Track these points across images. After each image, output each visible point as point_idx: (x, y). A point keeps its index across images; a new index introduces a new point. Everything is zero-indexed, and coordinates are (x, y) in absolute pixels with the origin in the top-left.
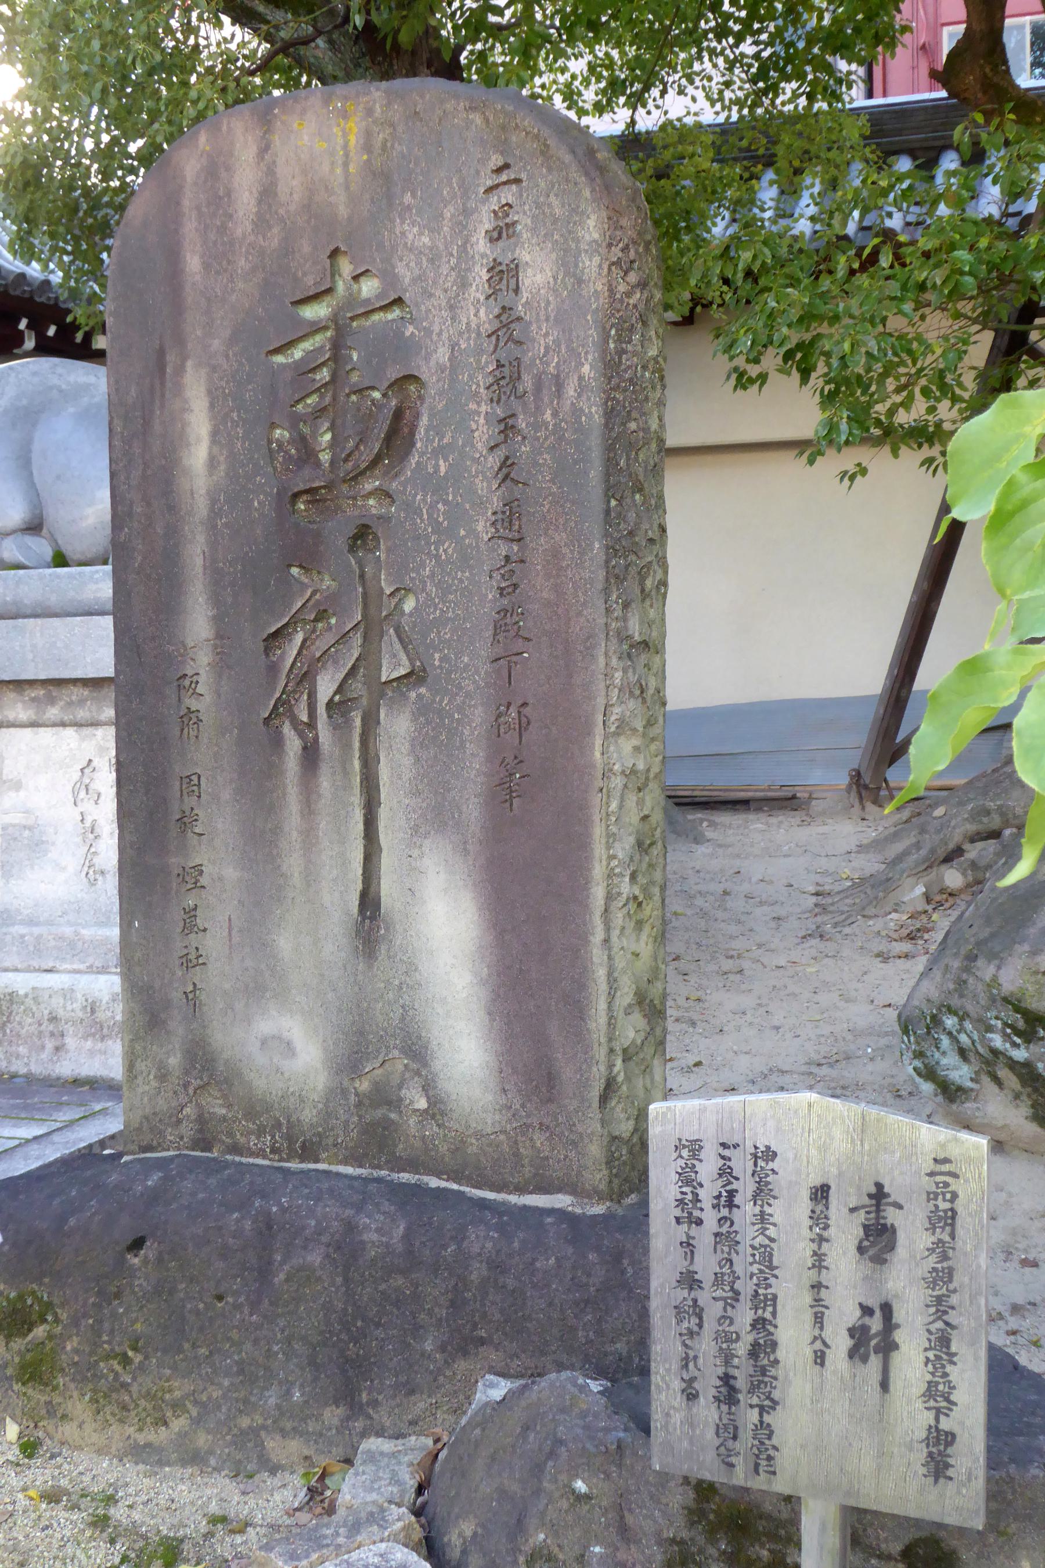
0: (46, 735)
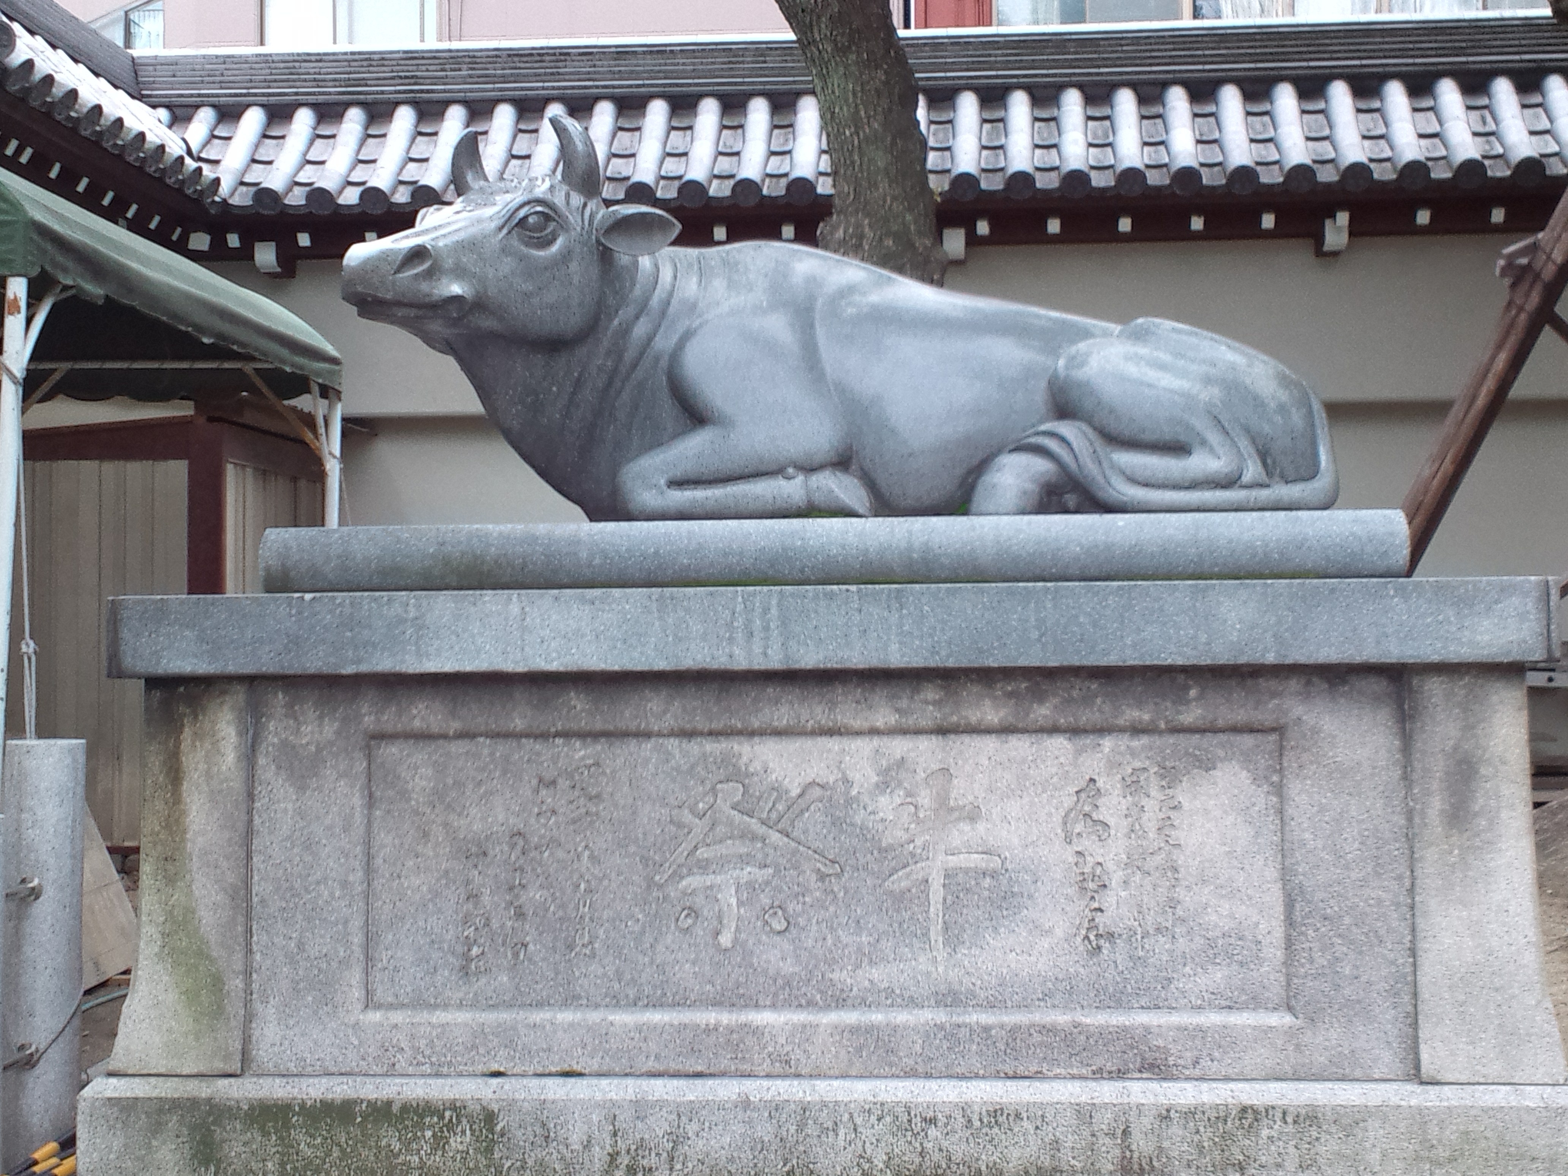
0: (1019, 746)
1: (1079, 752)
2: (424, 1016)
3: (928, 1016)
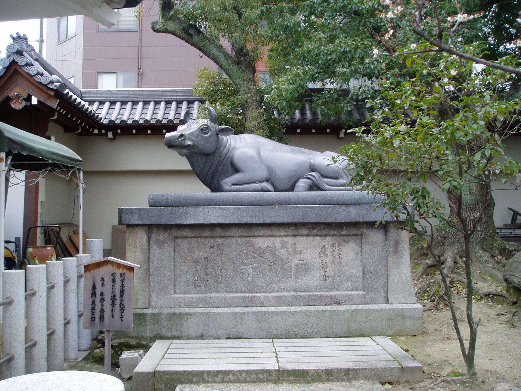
0: (310, 239)
1: (322, 240)
2: (187, 295)
3: (291, 294)
